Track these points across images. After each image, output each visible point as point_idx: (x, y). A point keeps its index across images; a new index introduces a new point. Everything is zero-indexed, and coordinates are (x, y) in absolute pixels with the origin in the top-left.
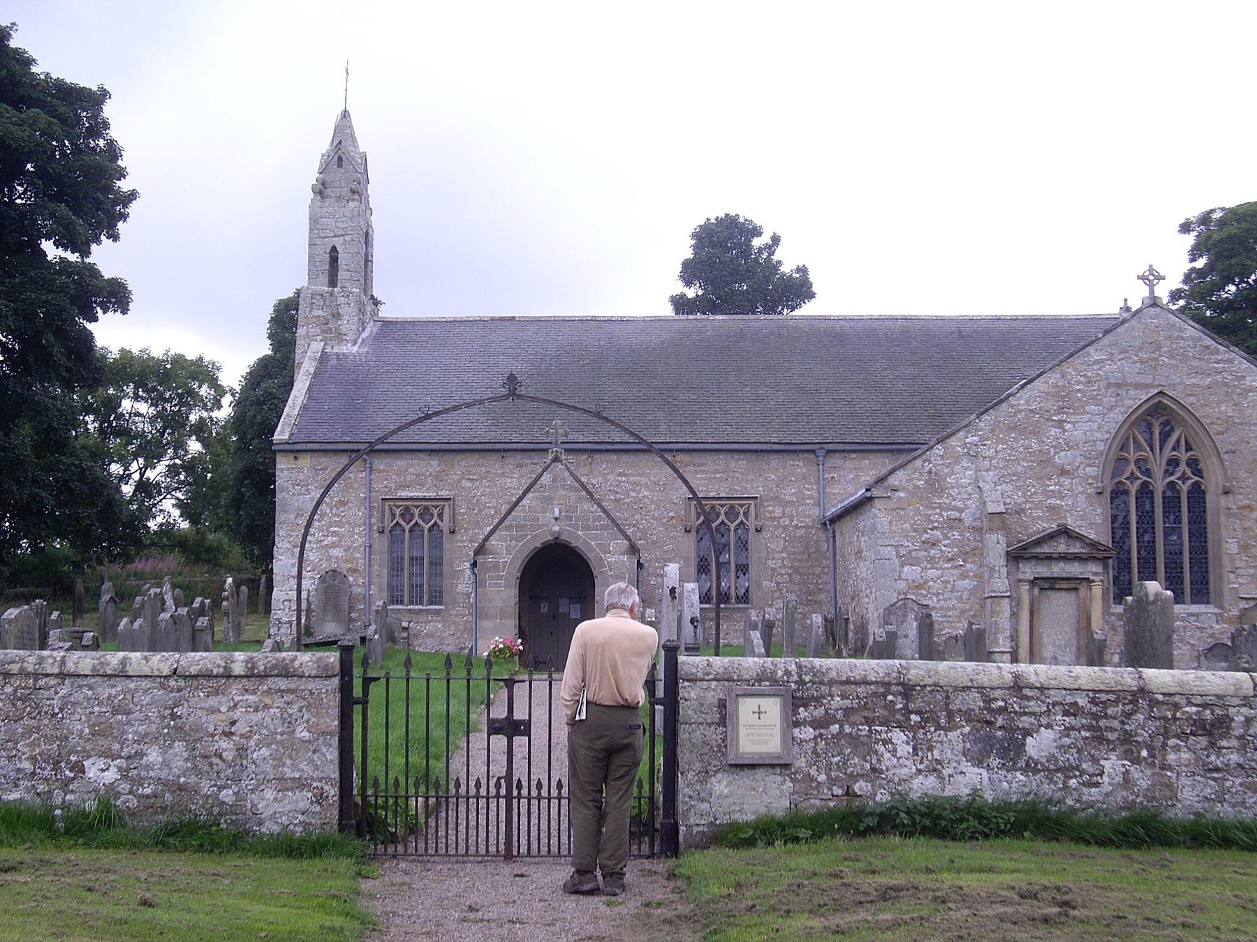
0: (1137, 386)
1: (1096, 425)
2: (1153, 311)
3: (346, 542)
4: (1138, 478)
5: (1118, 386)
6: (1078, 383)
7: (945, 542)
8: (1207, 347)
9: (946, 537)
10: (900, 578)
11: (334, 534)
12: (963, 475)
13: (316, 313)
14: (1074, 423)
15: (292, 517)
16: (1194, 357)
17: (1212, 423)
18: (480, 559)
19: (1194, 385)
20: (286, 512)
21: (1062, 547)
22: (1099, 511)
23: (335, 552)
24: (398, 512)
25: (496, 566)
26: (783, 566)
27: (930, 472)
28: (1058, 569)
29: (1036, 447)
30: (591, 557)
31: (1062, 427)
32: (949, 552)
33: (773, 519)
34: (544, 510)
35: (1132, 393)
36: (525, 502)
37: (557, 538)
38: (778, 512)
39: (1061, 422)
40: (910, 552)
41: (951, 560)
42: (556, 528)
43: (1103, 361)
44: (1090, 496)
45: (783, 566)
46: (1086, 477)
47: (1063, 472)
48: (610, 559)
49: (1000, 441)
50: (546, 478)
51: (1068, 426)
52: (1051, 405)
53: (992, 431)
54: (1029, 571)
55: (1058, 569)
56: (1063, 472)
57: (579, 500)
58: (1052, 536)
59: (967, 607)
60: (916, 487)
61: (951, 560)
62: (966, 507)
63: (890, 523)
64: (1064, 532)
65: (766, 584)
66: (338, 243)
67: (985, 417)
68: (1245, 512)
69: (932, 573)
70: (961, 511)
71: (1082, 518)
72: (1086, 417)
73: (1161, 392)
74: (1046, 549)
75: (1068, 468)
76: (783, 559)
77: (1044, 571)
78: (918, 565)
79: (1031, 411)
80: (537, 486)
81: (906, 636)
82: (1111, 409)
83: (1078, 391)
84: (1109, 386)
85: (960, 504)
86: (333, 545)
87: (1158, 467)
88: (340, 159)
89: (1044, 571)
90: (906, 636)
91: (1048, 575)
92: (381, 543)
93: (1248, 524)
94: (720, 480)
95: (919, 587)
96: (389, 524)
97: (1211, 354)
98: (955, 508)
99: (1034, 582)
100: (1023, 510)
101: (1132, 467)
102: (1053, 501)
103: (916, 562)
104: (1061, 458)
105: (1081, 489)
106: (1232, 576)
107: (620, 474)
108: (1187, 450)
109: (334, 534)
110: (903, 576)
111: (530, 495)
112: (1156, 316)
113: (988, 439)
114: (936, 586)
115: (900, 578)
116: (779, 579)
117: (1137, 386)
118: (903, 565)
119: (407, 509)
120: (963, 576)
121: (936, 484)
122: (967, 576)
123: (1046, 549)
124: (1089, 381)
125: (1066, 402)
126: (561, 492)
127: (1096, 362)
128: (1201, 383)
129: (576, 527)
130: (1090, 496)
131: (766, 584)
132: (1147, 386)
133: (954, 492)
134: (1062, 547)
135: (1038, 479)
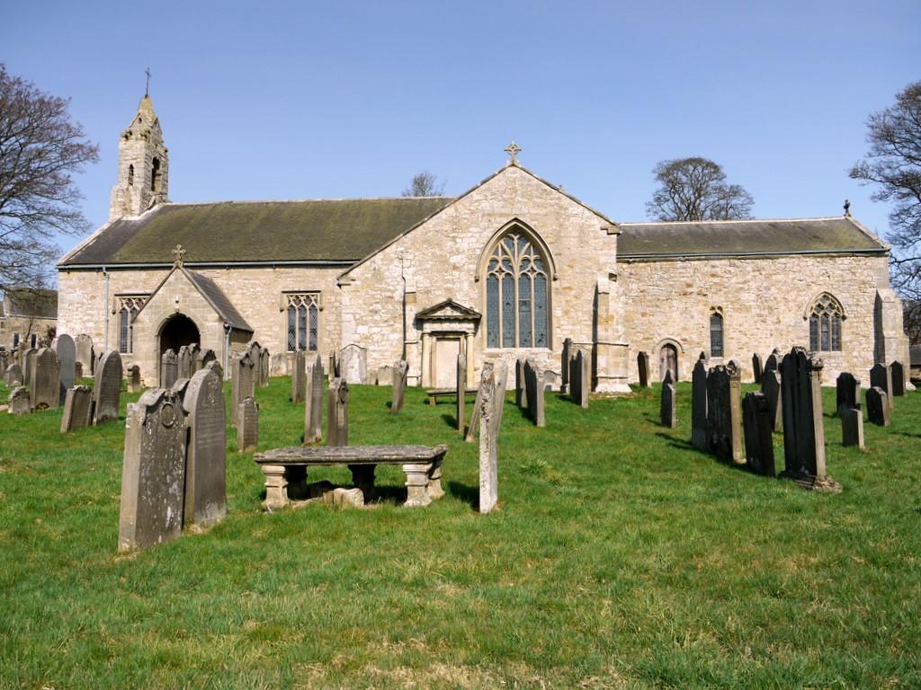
0: (502, 215)
1: (475, 240)
2: (514, 169)
3: (95, 319)
4: (503, 271)
5: (490, 215)
6: (466, 213)
7: (383, 311)
8: (545, 190)
9: (383, 308)
10: (356, 333)
11: (89, 315)
12: (394, 270)
13: (119, 200)
14: (462, 238)
15: (67, 305)
16: (537, 197)
17: (547, 237)
18: (134, 326)
19: (536, 214)
20: (63, 303)
21: (448, 312)
22: (477, 291)
23: (90, 325)
24: (124, 301)
25: (143, 330)
26: (335, 330)
27: (375, 269)
28: (446, 327)
29: (438, 253)
30: (197, 323)
31: (455, 241)
32: (385, 317)
33: (330, 303)
34: (171, 297)
35: (498, 219)
36: (160, 292)
37: (177, 313)
38: (333, 299)
39: (454, 237)
40: (362, 317)
41: (386, 321)
42: (177, 307)
43: (481, 200)
44: (471, 282)
45: (335, 330)
46: (469, 271)
47: (455, 268)
48: (207, 324)
49: (417, 250)
50: (172, 278)
51: (458, 240)
52: (447, 227)
53: (412, 244)
54: (428, 327)
55: (446, 327)
56: (455, 268)
57: (190, 290)
58: (441, 307)
59: (395, 350)
60: (367, 278)
61: (386, 321)
62: (396, 290)
63: (350, 299)
64: (449, 304)
65: (325, 339)
66: (133, 162)
67: (408, 235)
68: (567, 291)
69: (376, 330)
70: (393, 292)
71: (467, 295)
72: (470, 235)
73: (516, 219)
74: (439, 314)
75: (457, 265)
76: (335, 325)
77: (437, 327)
78: (367, 324)
79: (437, 231)
80: (166, 283)
81: (353, 367)
82: (485, 230)
83: (465, 219)
84: (483, 216)
85: (392, 288)
86: (88, 321)
87: (516, 264)
88: (140, 119)
89: (437, 327)
90: (353, 367)
91: (440, 330)
92: (115, 319)
93: (569, 298)
94: (300, 282)
95: (366, 338)
96: (119, 308)
97: (548, 194)
98: (389, 291)
99: (433, 334)
100: (430, 291)
101: (500, 264)
102: (449, 285)
103: (364, 323)
104: (454, 259)
105: (465, 278)
106: (558, 330)
107: (245, 279)
108: (526, 253)
109: (89, 315)
110: (358, 332)
111: (162, 288)
112: (515, 172)
113: (410, 248)
114: (376, 338)
115: (356, 333)
116: (333, 337)
117: (502, 215)
118: (357, 325)
119: (129, 300)
120: (394, 331)
121: (378, 275)
122: (396, 331)
123: (439, 314)
124: (472, 213)
125: (457, 226)
126: (181, 286)
127: (477, 201)
128: (541, 212)
129: (188, 306)
130: (471, 282)
131: (325, 339)
132: (508, 215)
133: (389, 281)
134: (448, 312)
135: (439, 271)
